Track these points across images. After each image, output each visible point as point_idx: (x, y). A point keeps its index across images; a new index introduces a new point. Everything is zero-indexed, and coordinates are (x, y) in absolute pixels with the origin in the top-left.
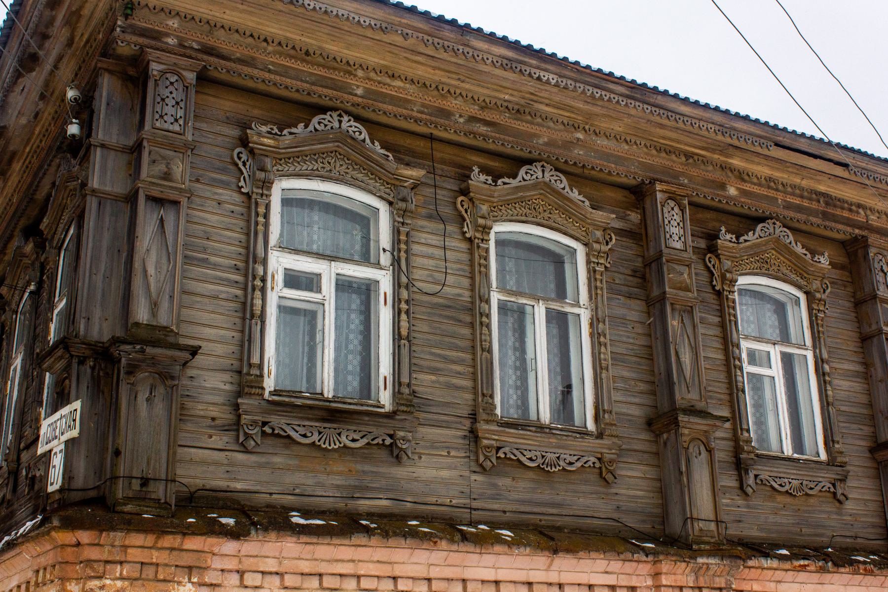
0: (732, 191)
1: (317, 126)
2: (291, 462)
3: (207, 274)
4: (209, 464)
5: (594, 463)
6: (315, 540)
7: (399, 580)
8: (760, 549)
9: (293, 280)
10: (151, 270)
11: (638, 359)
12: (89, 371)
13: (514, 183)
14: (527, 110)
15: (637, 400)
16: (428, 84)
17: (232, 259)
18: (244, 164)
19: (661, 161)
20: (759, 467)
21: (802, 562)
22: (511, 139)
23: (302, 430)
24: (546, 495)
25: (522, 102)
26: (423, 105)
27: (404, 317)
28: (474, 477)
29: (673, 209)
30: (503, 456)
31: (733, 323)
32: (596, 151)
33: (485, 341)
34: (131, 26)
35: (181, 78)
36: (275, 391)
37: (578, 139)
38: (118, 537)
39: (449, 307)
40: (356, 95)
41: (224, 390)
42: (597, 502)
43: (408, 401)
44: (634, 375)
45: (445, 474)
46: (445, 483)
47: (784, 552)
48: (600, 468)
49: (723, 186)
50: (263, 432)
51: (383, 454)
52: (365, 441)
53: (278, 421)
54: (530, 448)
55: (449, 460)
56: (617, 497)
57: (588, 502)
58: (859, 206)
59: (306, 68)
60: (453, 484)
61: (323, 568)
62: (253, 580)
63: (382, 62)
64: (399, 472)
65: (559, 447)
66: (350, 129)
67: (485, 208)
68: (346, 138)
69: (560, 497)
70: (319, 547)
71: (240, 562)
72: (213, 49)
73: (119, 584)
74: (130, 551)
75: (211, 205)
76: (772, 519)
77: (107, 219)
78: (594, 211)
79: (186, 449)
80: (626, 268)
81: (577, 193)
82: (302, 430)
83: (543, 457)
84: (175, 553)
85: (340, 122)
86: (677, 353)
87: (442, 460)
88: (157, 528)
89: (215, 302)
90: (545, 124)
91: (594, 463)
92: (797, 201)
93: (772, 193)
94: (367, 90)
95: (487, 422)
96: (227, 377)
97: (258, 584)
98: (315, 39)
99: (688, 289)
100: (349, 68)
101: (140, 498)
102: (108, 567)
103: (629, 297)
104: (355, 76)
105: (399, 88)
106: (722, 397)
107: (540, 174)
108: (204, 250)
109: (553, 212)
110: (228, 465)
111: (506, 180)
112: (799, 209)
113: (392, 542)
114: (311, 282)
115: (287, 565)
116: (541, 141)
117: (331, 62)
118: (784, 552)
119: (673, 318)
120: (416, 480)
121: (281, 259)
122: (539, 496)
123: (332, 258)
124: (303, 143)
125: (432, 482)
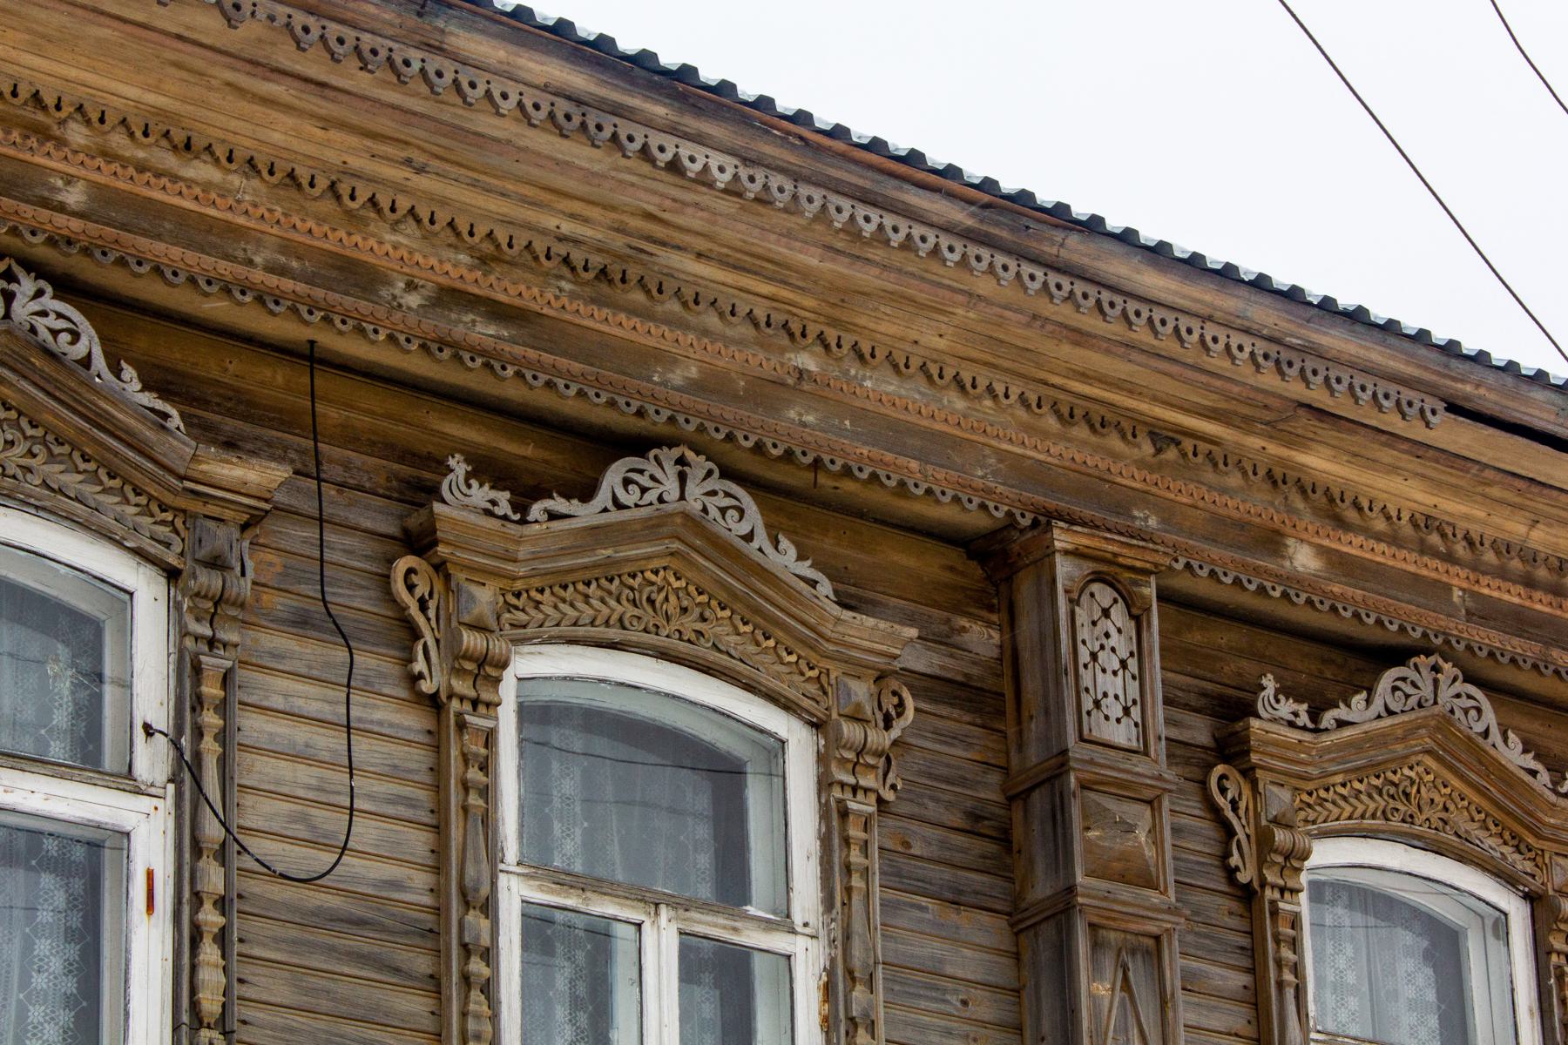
0: (1304, 559)
13: (585, 514)
14: (633, 272)
16: (303, 174)
19: (1073, 452)
22: (576, 367)
25: (619, 242)
26: (286, 247)
27: (210, 952)
29: (1106, 613)
31: (1290, 993)
32: (859, 415)
37: (801, 373)
39: (361, 923)
40: (61, 208)
49: (1272, 542)
63: (151, 98)
66: (40, 323)
78: (847, 615)
80: (949, 805)
93: (1431, 569)
94: (99, 193)
103: (955, 900)
104: (61, 143)
105: (207, 186)
107: (671, 487)
111: (559, 504)
116: (677, 377)
119: (1097, 972)
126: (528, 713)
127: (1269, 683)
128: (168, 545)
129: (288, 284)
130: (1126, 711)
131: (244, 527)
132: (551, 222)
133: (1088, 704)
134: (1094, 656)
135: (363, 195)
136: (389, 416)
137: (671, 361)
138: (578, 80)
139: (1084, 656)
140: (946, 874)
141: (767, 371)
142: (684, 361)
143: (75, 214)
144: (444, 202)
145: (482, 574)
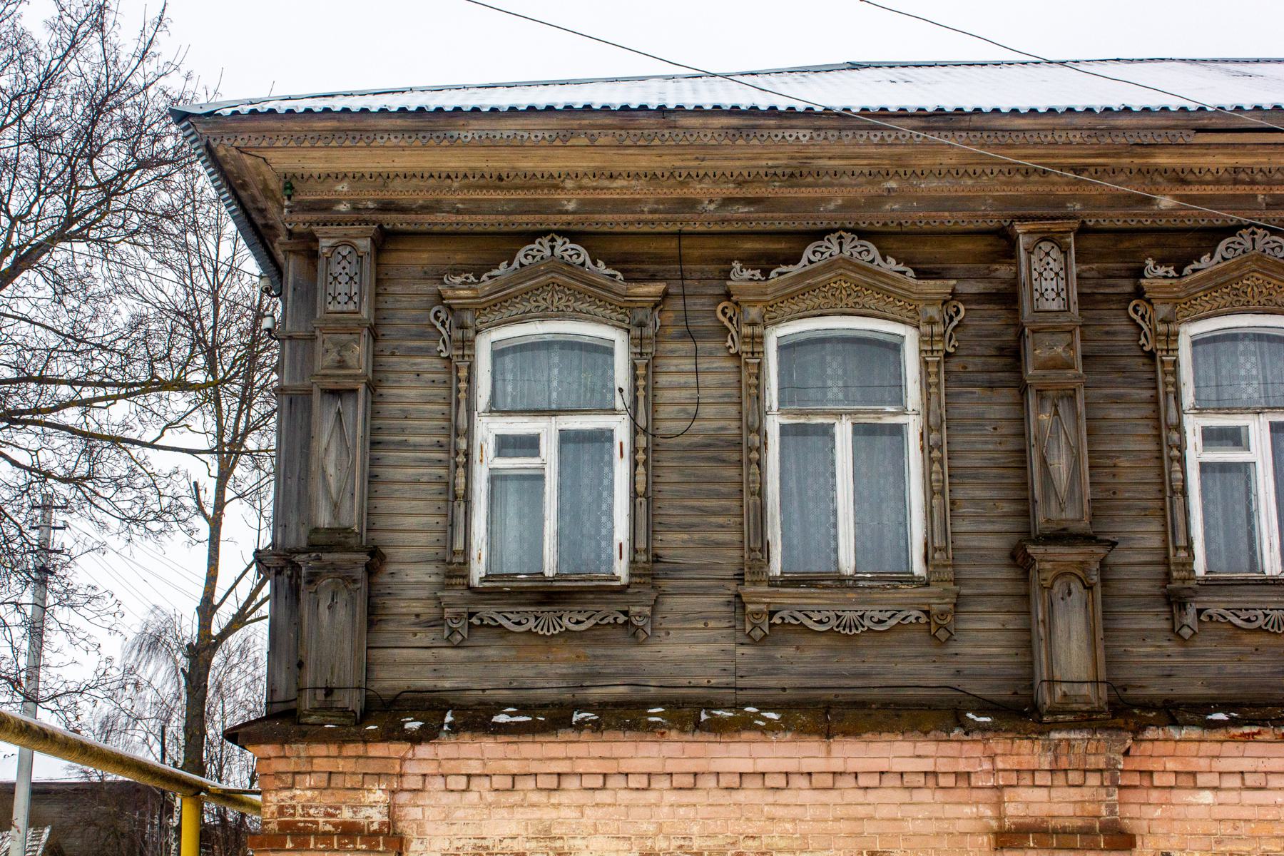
0: (1166, 202)
1: (524, 261)
2: (507, 654)
3: (406, 458)
4: (414, 664)
5: (917, 618)
6: (514, 739)
7: (1037, 774)
8: (1177, 712)
9: (506, 445)
10: (331, 470)
11: (1001, 471)
12: (286, 580)
13: (794, 270)
14: (805, 171)
15: (996, 527)
16: (659, 173)
17: (434, 435)
18: (443, 324)
19: (1034, 189)
20: (1205, 599)
21: (1247, 730)
22: (782, 215)
23: (515, 618)
24: (847, 663)
25: (794, 163)
26: (658, 201)
27: (641, 469)
28: (740, 650)
29: (1048, 254)
30: (779, 621)
31: (1171, 397)
32: (918, 199)
33: (754, 482)
34: (299, 203)
36: (487, 576)
37: (889, 190)
38: (301, 748)
39: (709, 445)
40: (567, 212)
41: (429, 583)
42: (924, 667)
43: (651, 568)
44: (994, 494)
45: (702, 649)
46: (702, 661)
48: (928, 623)
49: (1148, 201)
50: (471, 625)
51: (619, 634)
52: (593, 621)
53: (487, 611)
54: (819, 606)
55: (707, 633)
56: (958, 659)
59: (499, 195)
60: (711, 661)
61: (535, 767)
62: (457, 783)
63: (592, 164)
65: (863, 603)
66: (565, 254)
67: (754, 313)
68: (565, 266)
69: (866, 665)
70: (522, 746)
71: (440, 766)
72: (391, 202)
73: (309, 793)
74: (315, 761)
75: (408, 379)
76: (1230, 668)
77: (299, 416)
78: (921, 282)
79: (396, 651)
80: (987, 347)
81: (894, 261)
82: (515, 618)
83: (838, 617)
84: (361, 761)
85: (552, 248)
86: (1044, 461)
87: (696, 633)
88: (339, 738)
89: (417, 486)
90: (836, 182)
91: (917, 618)
93: (1242, 190)
94: (582, 203)
95: (754, 583)
96: (431, 568)
97: (420, 787)
98: (503, 161)
99: (1069, 366)
100: (553, 182)
101: (326, 708)
102: (298, 777)
103: (991, 386)
104: (563, 188)
105: (622, 188)
106: (1150, 504)
107: (836, 249)
108: (403, 430)
109: (865, 293)
110: (435, 663)
111: (783, 269)
113: (607, 735)
114: (530, 444)
115: (492, 767)
116: (832, 206)
117: (530, 181)
119: (1041, 408)
120: (663, 660)
121: (491, 426)
122: (836, 666)
125: (684, 661)
126: (781, 349)
127: (1150, 263)
128: (623, 321)
129: (657, 216)
130: (1058, 294)
131: (654, 308)
132: (764, 163)
133: (1037, 295)
134: (1041, 274)
135: (684, 174)
136: (720, 247)
137: (829, 200)
138: (734, 121)
139: (1035, 275)
140: (985, 376)
141: (873, 192)
142: (833, 199)
143: (573, 213)
144: (717, 168)
145: (752, 303)
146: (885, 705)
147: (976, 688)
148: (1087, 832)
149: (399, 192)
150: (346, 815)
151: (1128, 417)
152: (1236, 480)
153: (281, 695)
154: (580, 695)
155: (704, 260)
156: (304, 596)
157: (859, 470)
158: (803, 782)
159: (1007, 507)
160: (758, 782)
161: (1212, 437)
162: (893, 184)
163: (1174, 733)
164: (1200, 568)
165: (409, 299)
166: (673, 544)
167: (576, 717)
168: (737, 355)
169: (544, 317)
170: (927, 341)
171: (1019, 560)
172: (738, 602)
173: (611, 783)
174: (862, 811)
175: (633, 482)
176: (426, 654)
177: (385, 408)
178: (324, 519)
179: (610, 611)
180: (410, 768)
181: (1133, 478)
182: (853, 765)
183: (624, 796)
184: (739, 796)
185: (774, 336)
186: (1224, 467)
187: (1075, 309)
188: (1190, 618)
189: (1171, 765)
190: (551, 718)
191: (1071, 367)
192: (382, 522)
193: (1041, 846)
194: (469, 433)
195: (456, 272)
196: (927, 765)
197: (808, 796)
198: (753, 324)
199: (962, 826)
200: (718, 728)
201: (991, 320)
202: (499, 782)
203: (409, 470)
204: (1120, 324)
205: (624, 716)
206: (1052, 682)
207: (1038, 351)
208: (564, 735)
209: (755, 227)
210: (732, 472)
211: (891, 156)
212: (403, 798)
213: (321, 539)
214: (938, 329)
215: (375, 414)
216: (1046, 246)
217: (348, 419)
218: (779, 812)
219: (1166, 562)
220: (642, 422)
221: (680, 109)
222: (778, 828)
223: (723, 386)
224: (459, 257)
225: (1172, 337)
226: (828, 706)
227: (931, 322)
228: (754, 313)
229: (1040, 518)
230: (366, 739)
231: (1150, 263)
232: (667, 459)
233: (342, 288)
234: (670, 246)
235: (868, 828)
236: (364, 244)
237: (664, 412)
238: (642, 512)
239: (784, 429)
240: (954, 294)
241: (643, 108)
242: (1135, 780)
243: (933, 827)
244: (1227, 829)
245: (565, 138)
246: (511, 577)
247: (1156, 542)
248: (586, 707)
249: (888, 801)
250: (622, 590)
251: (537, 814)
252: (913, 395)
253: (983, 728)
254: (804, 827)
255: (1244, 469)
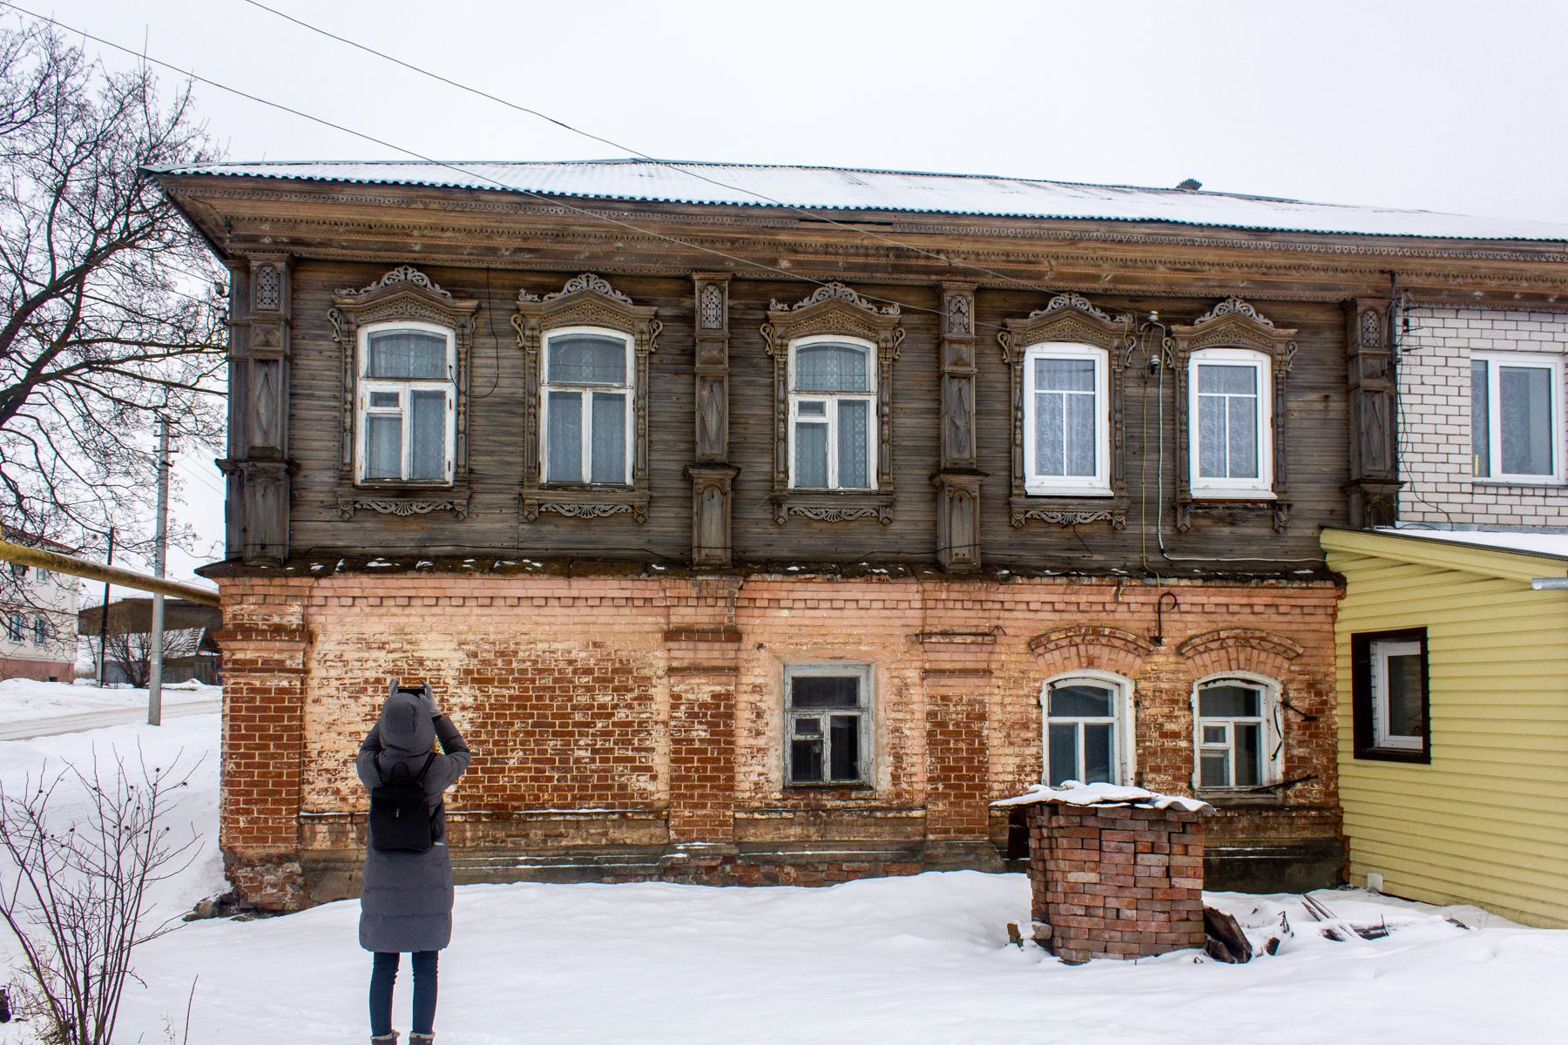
8: (774, 565)
9: (378, 399)
10: (262, 410)
13: (558, 296)
32: (637, 255)
35: (274, 268)
38: (246, 580)
43: (468, 477)
45: (498, 526)
46: (499, 532)
47: (795, 568)
49: (774, 262)
51: (448, 516)
53: (366, 500)
54: (568, 502)
57: (621, 538)
58: (938, 252)
59: (367, 238)
64: (460, 527)
68: (413, 286)
76: (804, 541)
86: (703, 419)
88: (269, 574)
92: (861, 260)
96: (330, 473)
100: (405, 231)
108: (311, 387)
109: (431, 310)
112: (864, 268)
113: (437, 575)
114: (392, 399)
117: (390, 230)
118: (795, 568)
119: (703, 388)
123: (408, 379)
124: (378, 296)
127: (773, 301)
138: (517, 199)
142: (584, 252)
145: (533, 316)
146: (605, 560)
147: (659, 551)
148: (715, 632)
149: (303, 232)
150: (276, 620)
151: (755, 395)
152: (818, 431)
153: (234, 549)
154: (424, 551)
155: (503, 287)
156: (246, 489)
157: (594, 419)
158: (556, 603)
159: (682, 446)
160: (529, 603)
161: (804, 407)
162: (620, 245)
163: (768, 577)
164: (791, 484)
165: (313, 302)
166: (482, 463)
167: (419, 564)
168: (523, 348)
169: (401, 318)
170: (639, 343)
171: (687, 478)
172: (520, 498)
173: (441, 602)
174: (590, 619)
175: (457, 425)
176: (325, 525)
177: (300, 373)
178: (258, 441)
179: (442, 502)
180: (316, 592)
181: (755, 431)
182: (584, 594)
183: (449, 610)
184: (517, 610)
185: (363, 335)
186: (813, 426)
187: (726, 328)
188: (784, 512)
189: (766, 595)
190: (403, 564)
191: (721, 363)
192: (298, 444)
193: (688, 639)
194: (353, 390)
195: (344, 288)
196: (627, 594)
197: (558, 611)
198: (533, 329)
199: (646, 628)
200: (504, 571)
201: (677, 332)
202: (372, 601)
203: (316, 412)
204: (755, 339)
205: (449, 564)
206: (700, 547)
207: (704, 353)
208: (411, 574)
209: (534, 267)
210: (518, 420)
211: (619, 227)
212: (313, 610)
213: (256, 453)
214: (645, 337)
215: (293, 376)
216: (711, 288)
217: (272, 379)
218: (541, 619)
219: (772, 481)
220: (463, 388)
221: (480, 189)
222: (541, 629)
223: (514, 367)
224: (346, 277)
225: (784, 347)
226: (573, 560)
227: (642, 333)
228: (533, 322)
229: (699, 452)
230: (287, 575)
231: (773, 301)
232: (478, 411)
233: (267, 294)
234: (482, 277)
235: (593, 628)
236: (281, 266)
237: (478, 381)
238: (462, 442)
239: (552, 396)
240: (656, 315)
241: (457, 187)
242: (746, 603)
243: (631, 628)
244: (795, 630)
245: (407, 204)
246: (381, 480)
247: (767, 468)
248: (427, 558)
249: (604, 614)
250: (449, 490)
251: (396, 620)
252: (873, 385)
253: (659, 573)
254: (555, 628)
255: (823, 427)
